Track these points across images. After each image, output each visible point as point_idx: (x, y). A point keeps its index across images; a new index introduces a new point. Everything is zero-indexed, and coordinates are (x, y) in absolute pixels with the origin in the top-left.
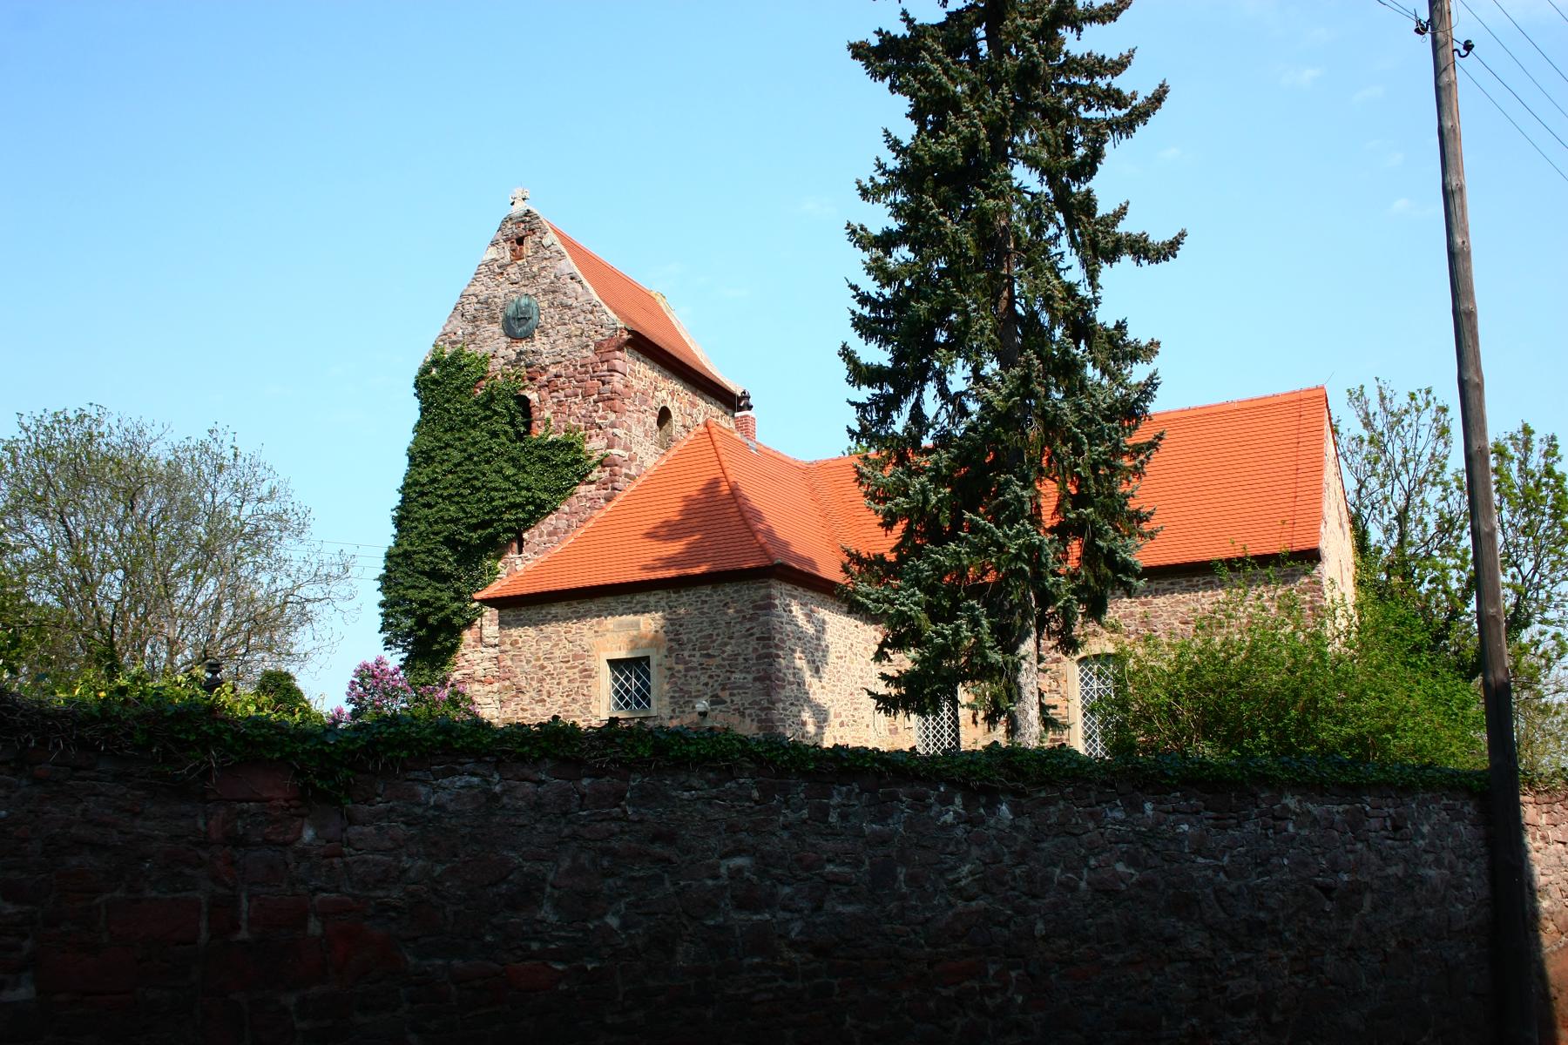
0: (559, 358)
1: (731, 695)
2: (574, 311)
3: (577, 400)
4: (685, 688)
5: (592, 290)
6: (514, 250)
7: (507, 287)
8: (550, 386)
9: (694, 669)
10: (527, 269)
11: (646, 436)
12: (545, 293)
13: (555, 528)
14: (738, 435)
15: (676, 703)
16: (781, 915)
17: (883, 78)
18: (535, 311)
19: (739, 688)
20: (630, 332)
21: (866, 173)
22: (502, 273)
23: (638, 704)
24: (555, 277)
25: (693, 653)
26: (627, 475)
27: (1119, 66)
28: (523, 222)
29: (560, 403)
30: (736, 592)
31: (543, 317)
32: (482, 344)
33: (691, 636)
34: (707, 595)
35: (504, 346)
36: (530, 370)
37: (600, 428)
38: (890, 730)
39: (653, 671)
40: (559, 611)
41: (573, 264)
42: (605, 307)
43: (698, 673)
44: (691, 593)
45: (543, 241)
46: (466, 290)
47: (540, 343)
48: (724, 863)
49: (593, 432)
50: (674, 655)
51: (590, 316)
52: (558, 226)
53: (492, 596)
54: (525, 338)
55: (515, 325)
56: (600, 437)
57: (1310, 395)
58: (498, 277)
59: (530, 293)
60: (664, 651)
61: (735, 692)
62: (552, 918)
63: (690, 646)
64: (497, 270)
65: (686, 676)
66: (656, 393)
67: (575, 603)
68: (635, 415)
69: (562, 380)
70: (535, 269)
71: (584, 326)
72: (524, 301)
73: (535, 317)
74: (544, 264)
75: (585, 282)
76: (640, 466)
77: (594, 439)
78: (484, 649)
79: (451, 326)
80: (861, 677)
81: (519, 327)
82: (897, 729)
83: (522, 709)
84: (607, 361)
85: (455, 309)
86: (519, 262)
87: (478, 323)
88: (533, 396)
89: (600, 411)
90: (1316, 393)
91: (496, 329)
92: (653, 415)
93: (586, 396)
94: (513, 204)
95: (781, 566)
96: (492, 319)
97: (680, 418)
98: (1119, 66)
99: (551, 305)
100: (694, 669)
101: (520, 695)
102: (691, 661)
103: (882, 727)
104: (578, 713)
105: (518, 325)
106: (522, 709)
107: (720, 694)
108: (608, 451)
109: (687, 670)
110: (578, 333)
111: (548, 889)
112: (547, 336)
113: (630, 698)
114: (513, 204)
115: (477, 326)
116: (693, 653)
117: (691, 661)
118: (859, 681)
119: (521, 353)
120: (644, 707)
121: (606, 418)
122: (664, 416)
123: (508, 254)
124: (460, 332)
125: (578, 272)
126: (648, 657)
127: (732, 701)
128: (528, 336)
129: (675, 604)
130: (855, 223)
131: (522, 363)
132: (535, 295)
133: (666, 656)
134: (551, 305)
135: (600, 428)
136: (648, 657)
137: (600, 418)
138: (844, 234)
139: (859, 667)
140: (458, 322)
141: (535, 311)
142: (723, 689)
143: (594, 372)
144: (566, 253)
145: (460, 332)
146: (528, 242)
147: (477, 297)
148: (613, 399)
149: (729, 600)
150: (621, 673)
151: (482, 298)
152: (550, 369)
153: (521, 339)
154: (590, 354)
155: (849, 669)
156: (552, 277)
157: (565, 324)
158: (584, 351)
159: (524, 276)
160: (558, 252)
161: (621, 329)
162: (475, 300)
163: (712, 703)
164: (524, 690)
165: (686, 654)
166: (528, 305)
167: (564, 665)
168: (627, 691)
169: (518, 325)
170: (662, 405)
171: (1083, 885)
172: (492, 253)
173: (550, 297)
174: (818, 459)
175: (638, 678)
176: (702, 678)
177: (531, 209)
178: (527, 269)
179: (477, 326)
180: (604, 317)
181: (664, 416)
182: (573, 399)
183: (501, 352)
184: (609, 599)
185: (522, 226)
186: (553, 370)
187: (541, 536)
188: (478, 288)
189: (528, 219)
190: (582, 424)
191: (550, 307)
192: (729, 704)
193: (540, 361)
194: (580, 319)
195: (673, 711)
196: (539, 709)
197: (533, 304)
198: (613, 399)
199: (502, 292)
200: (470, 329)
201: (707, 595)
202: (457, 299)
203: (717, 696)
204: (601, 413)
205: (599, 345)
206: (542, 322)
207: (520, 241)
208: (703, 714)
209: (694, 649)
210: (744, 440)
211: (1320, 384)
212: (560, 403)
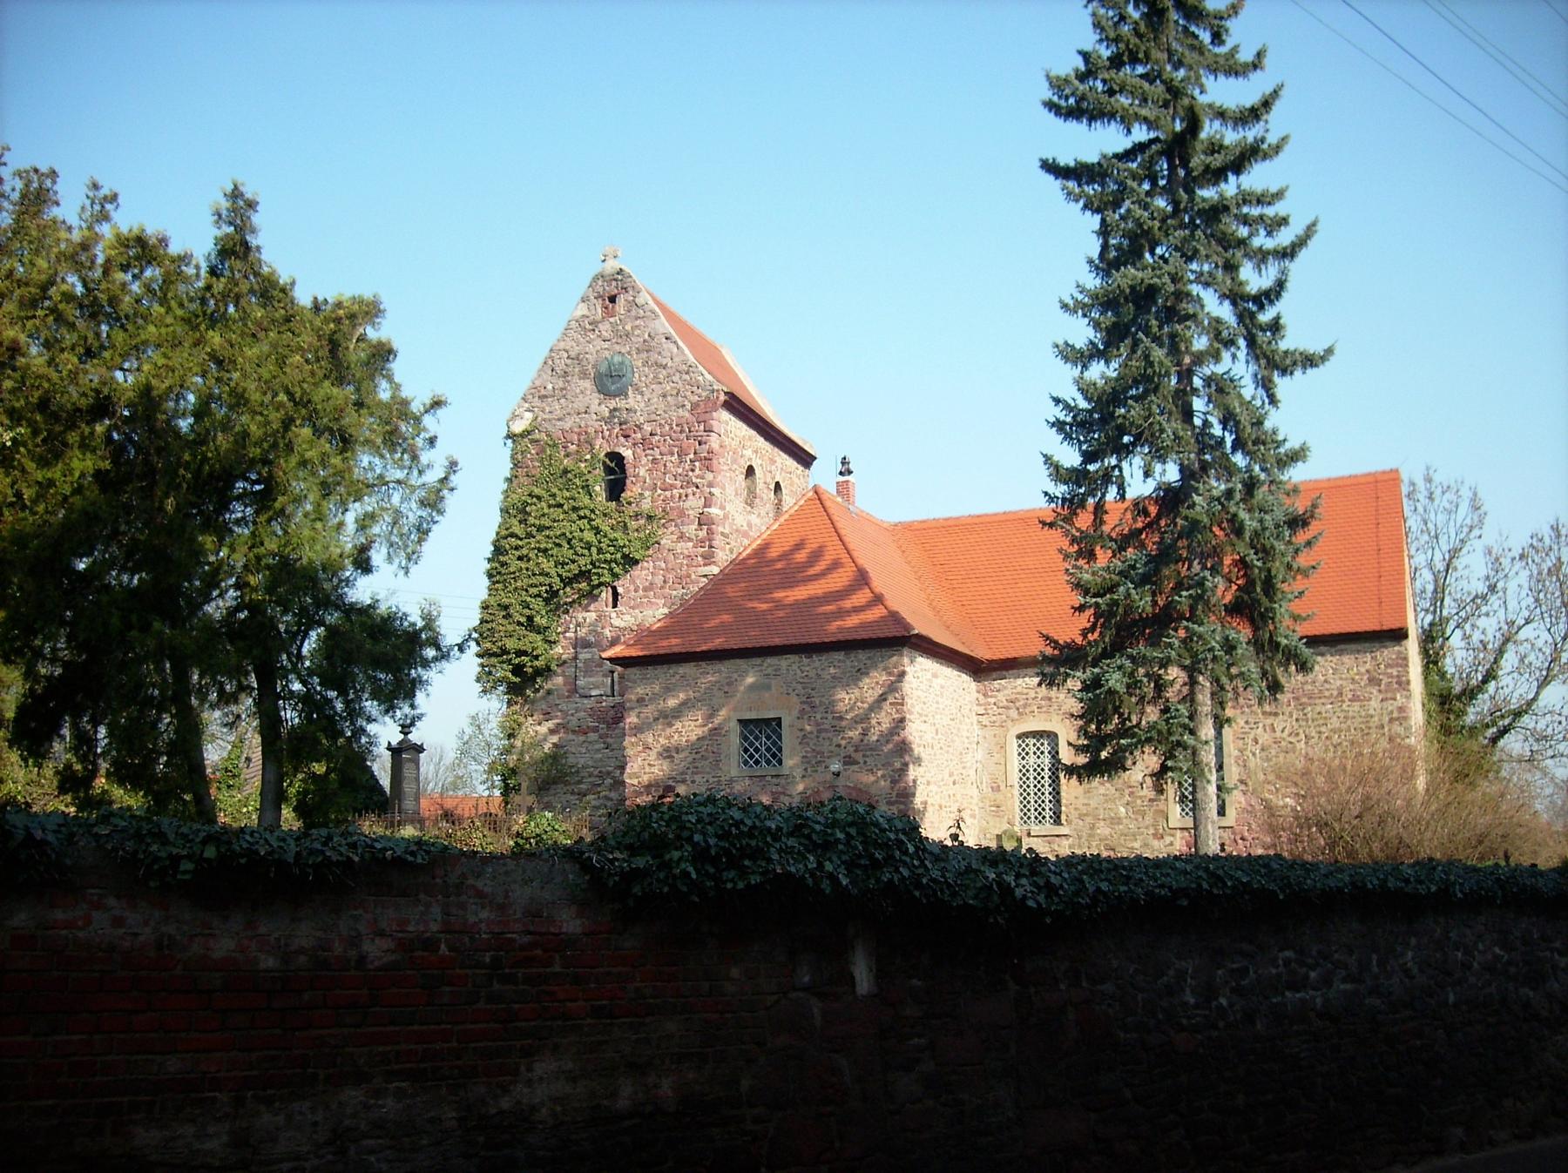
0: (653, 417)
1: (864, 756)
2: (669, 371)
3: (673, 459)
4: (818, 749)
5: (687, 351)
6: (606, 308)
7: (600, 344)
8: (645, 443)
9: (826, 731)
10: (621, 328)
11: (737, 494)
12: (639, 351)
13: (651, 584)
14: (839, 499)
15: (808, 763)
16: (1311, 992)
17: (1077, 201)
18: (629, 369)
19: (871, 749)
20: (726, 393)
21: (1068, 293)
22: (594, 330)
23: (769, 762)
24: (649, 336)
25: (825, 715)
26: (722, 534)
27: (1279, 195)
28: (616, 280)
29: (654, 461)
30: (869, 658)
31: (636, 375)
32: (573, 399)
33: (823, 699)
34: (839, 661)
35: (597, 401)
36: (624, 427)
37: (697, 487)
38: (992, 788)
39: (785, 732)
40: (687, 671)
41: (667, 324)
42: (701, 368)
43: (830, 735)
44: (824, 658)
45: (637, 300)
46: (556, 345)
47: (633, 400)
48: (1280, 955)
49: (690, 491)
50: (806, 717)
51: (687, 377)
52: (651, 291)
53: (620, 655)
54: (618, 396)
55: (608, 382)
56: (697, 496)
57: (1386, 477)
58: (589, 334)
59: (623, 351)
60: (795, 713)
61: (868, 753)
62: (1192, 1001)
63: (822, 709)
64: (588, 326)
65: (818, 737)
66: (745, 452)
67: (703, 664)
68: (728, 475)
69: (657, 438)
70: (628, 327)
71: (680, 385)
72: (617, 359)
73: (629, 375)
74: (638, 322)
75: (681, 343)
76: (731, 525)
77: (691, 497)
78: (578, 700)
79: (540, 380)
80: (968, 738)
81: (613, 384)
82: (999, 786)
83: (649, 765)
84: (705, 422)
85: (545, 363)
86: (612, 320)
87: (569, 378)
88: (627, 453)
89: (697, 470)
90: (1392, 476)
91: (588, 384)
92: (742, 473)
93: (682, 454)
94: (604, 261)
95: (918, 636)
96: (584, 375)
97: (762, 476)
98: (1279, 195)
99: (646, 363)
100: (826, 731)
101: (647, 751)
102: (823, 723)
103: (984, 784)
104: (708, 770)
105: (610, 381)
106: (649, 765)
107: (853, 755)
108: (706, 510)
109: (819, 731)
110: (674, 392)
111: (1189, 980)
112: (642, 394)
113: (760, 756)
114: (604, 261)
115: (568, 382)
116: (825, 715)
117: (823, 723)
118: (966, 741)
119: (615, 409)
120: (774, 765)
121: (703, 478)
122: (750, 471)
123: (599, 311)
124: (550, 387)
125: (672, 332)
126: (780, 718)
127: (865, 762)
128: (622, 393)
129: (807, 669)
130: (1061, 342)
131: (616, 420)
132: (629, 353)
133: (798, 718)
134: (646, 363)
135: (697, 487)
136: (780, 718)
137: (697, 477)
138: (1050, 352)
139: (966, 728)
140: (547, 375)
141: (629, 369)
142: (856, 751)
143: (690, 431)
144: (660, 314)
145: (550, 387)
146: (621, 300)
147: (567, 352)
148: (710, 460)
149: (862, 666)
150: (751, 732)
151: (573, 354)
152: (645, 427)
153: (615, 396)
154: (687, 414)
155: (959, 729)
156: (646, 336)
157: (660, 383)
158: (680, 410)
159: (615, 332)
160: (653, 312)
161: (718, 391)
162: (566, 355)
163: (845, 763)
164: (651, 746)
165: (818, 716)
166: (622, 363)
167: (693, 724)
168: (757, 750)
169: (610, 381)
170: (748, 464)
171: (1475, 964)
172: (582, 310)
173: (644, 355)
174: (902, 520)
175: (768, 738)
176: (835, 739)
177: (623, 267)
178: (621, 328)
179: (568, 382)
180: (701, 378)
181: (750, 471)
182: (669, 458)
183: (594, 407)
184: (738, 661)
185: (614, 283)
186: (648, 428)
187: (636, 591)
188: (569, 344)
189: (620, 277)
190: (678, 483)
191: (644, 366)
192: (862, 764)
193: (635, 419)
194: (676, 378)
195: (806, 769)
196: (1156, 843)
197: (627, 362)
198: (710, 460)
199: (596, 350)
200: (561, 384)
201: (839, 661)
202: (546, 353)
203: (850, 757)
204: (697, 472)
205: (695, 406)
206: (635, 380)
207: (613, 299)
208: (837, 774)
209: (826, 712)
210: (846, 504)
211: (1394, 466)
212: (654, 461)
